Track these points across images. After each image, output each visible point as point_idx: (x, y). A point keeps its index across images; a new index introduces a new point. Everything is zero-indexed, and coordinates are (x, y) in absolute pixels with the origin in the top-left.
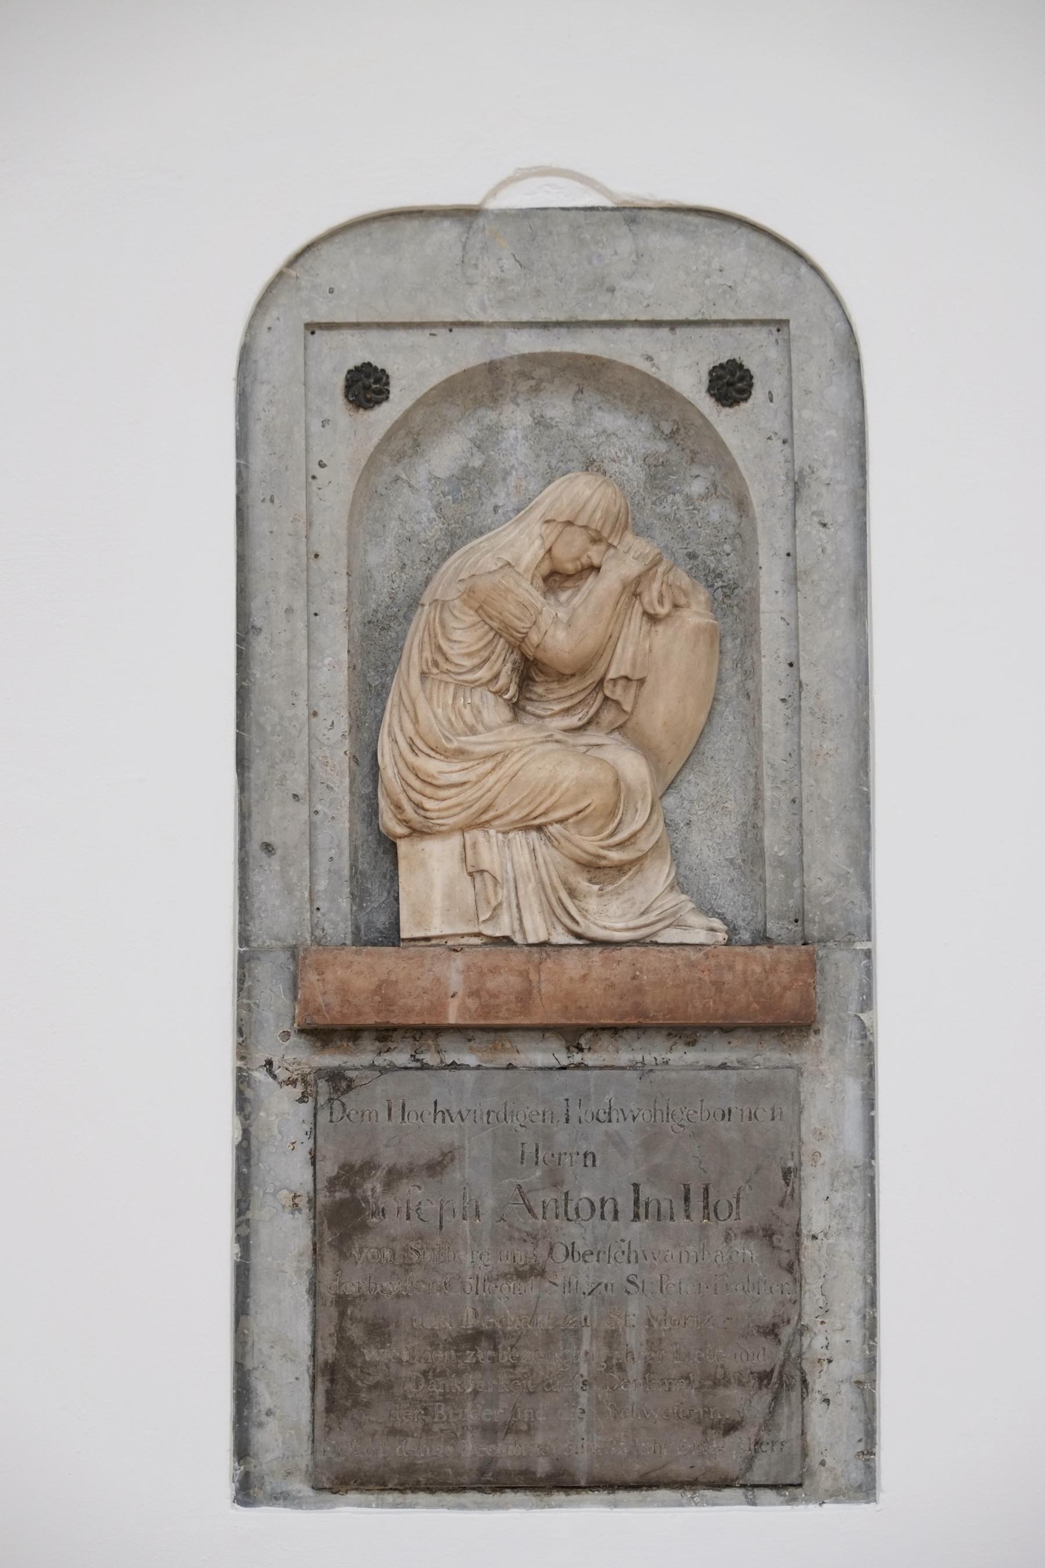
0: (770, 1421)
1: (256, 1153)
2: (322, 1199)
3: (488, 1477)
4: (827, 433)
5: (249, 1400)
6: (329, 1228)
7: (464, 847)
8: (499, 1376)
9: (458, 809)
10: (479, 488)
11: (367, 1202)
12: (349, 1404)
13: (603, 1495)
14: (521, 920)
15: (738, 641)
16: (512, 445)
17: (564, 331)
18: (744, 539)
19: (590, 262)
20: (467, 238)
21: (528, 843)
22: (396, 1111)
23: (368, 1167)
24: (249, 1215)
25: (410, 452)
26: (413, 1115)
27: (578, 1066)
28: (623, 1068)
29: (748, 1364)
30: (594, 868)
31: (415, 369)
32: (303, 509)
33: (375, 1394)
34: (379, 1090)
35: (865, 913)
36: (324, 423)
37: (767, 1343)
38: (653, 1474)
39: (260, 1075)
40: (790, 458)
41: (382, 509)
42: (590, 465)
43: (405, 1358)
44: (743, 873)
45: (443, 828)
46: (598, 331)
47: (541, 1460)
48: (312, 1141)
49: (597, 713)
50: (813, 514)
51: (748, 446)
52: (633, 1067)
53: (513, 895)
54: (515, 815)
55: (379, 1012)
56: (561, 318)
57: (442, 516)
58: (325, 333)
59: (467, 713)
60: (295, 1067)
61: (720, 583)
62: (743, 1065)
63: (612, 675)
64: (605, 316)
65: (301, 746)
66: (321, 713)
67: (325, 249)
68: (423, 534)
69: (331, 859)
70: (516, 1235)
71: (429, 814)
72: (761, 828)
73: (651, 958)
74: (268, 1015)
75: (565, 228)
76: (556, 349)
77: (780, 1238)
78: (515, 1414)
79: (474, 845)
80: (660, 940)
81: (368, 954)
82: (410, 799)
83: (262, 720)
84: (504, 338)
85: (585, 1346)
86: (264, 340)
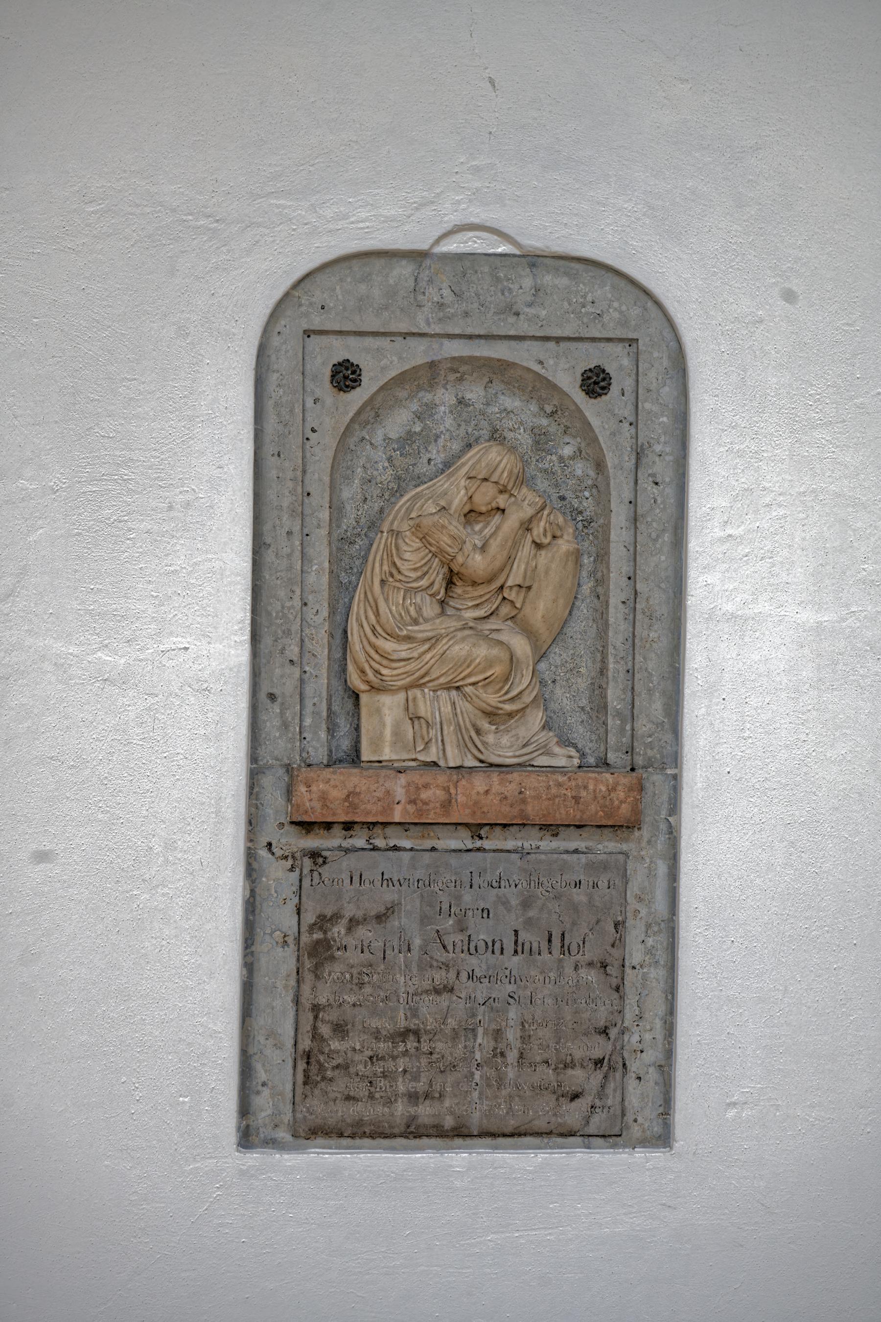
0: (601, 1093)
1: (259, 906)
2: (305, 939)
3: (412, 1129)
4: (661, 420)
5: (250, 1076)
6: (309, 958)
7: (407, 700)
8: (422, 1060)
9: (405, 676)
10: (419, 447)
11: (335, 941)
12: (319, 1079)
13: (488, 1141)
14: (444, 750)
15: (592, 559)
16: (442, 417)
17: (483, 341)
18: (601, 490)
19: (503, 294)
20: (419, 273)
21: (450, 699)
22: (356, 879)
23: (336, 917)
24: (253, 948)
25: (372, 421)
26: (367, 882)
27: (478, 850)
28: (508, 851)
29: (588, 1053)
30: (491, 715)
31: (378, 366)
32: (300, 461)
33: (337, 1072)
34: (345, 864)
35: (674, 749)
36: (315, 401)
37: (601, 1039)
38: (523, 1128)
39: (263, 853)
40: (634, 436)
41: (352, 460)
42: (496, 436)
43: (358, 1048)
44: (591, 717)
45: (394, 688)
46: (506, 343)
47: (448, 1117)
48: (298, 897)
49: (497, 608)
50: (649, 475)
51: (607, 427)
52: (515, 851)
53: (439, 734)
54: (442, 680)
55: (347, 813)
56: (482, 333)
57: (392, 465)
58: (318, 337)
59: (412, 609)
60: (288, 847)
61: (581, 518)
62: (589, 851)
63: (510, 583)
64: (512, 333)
65: (296, 627)
66: (309, 604)
67: (319, 278)
68: (379, 477)
69: (314, 704)
70: (435, 964)
71: (384, 678)
72: (606, 689)
73: (533, 783)
74: (270, 811)
75: (486, 269)
76: (477, 354)
77: (611, 969)
78: (431, 1085)
79: (415, 699)
80: (535, 764)
81: (341, 773)
82: (371, 667)
83: (269, 608)
84: (442, 344)
85: (479, 1040)
86: (276, 341)
